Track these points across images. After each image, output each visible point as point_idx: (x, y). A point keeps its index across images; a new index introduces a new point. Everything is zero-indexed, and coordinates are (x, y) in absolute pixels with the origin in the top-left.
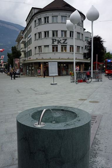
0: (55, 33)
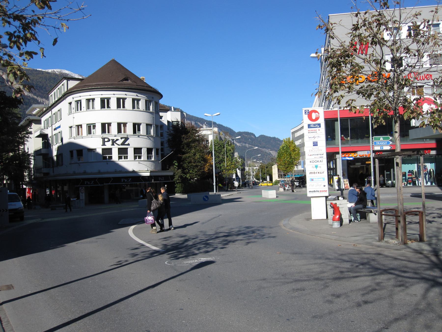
0: (105, 127)
